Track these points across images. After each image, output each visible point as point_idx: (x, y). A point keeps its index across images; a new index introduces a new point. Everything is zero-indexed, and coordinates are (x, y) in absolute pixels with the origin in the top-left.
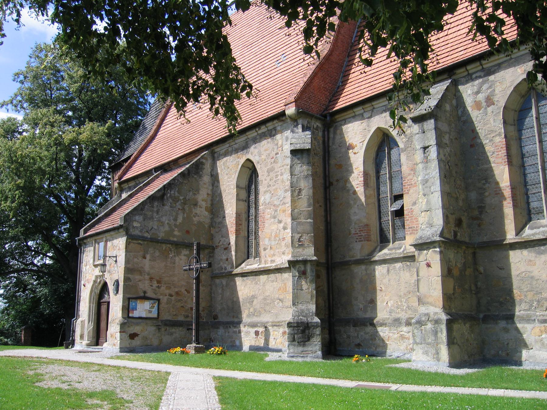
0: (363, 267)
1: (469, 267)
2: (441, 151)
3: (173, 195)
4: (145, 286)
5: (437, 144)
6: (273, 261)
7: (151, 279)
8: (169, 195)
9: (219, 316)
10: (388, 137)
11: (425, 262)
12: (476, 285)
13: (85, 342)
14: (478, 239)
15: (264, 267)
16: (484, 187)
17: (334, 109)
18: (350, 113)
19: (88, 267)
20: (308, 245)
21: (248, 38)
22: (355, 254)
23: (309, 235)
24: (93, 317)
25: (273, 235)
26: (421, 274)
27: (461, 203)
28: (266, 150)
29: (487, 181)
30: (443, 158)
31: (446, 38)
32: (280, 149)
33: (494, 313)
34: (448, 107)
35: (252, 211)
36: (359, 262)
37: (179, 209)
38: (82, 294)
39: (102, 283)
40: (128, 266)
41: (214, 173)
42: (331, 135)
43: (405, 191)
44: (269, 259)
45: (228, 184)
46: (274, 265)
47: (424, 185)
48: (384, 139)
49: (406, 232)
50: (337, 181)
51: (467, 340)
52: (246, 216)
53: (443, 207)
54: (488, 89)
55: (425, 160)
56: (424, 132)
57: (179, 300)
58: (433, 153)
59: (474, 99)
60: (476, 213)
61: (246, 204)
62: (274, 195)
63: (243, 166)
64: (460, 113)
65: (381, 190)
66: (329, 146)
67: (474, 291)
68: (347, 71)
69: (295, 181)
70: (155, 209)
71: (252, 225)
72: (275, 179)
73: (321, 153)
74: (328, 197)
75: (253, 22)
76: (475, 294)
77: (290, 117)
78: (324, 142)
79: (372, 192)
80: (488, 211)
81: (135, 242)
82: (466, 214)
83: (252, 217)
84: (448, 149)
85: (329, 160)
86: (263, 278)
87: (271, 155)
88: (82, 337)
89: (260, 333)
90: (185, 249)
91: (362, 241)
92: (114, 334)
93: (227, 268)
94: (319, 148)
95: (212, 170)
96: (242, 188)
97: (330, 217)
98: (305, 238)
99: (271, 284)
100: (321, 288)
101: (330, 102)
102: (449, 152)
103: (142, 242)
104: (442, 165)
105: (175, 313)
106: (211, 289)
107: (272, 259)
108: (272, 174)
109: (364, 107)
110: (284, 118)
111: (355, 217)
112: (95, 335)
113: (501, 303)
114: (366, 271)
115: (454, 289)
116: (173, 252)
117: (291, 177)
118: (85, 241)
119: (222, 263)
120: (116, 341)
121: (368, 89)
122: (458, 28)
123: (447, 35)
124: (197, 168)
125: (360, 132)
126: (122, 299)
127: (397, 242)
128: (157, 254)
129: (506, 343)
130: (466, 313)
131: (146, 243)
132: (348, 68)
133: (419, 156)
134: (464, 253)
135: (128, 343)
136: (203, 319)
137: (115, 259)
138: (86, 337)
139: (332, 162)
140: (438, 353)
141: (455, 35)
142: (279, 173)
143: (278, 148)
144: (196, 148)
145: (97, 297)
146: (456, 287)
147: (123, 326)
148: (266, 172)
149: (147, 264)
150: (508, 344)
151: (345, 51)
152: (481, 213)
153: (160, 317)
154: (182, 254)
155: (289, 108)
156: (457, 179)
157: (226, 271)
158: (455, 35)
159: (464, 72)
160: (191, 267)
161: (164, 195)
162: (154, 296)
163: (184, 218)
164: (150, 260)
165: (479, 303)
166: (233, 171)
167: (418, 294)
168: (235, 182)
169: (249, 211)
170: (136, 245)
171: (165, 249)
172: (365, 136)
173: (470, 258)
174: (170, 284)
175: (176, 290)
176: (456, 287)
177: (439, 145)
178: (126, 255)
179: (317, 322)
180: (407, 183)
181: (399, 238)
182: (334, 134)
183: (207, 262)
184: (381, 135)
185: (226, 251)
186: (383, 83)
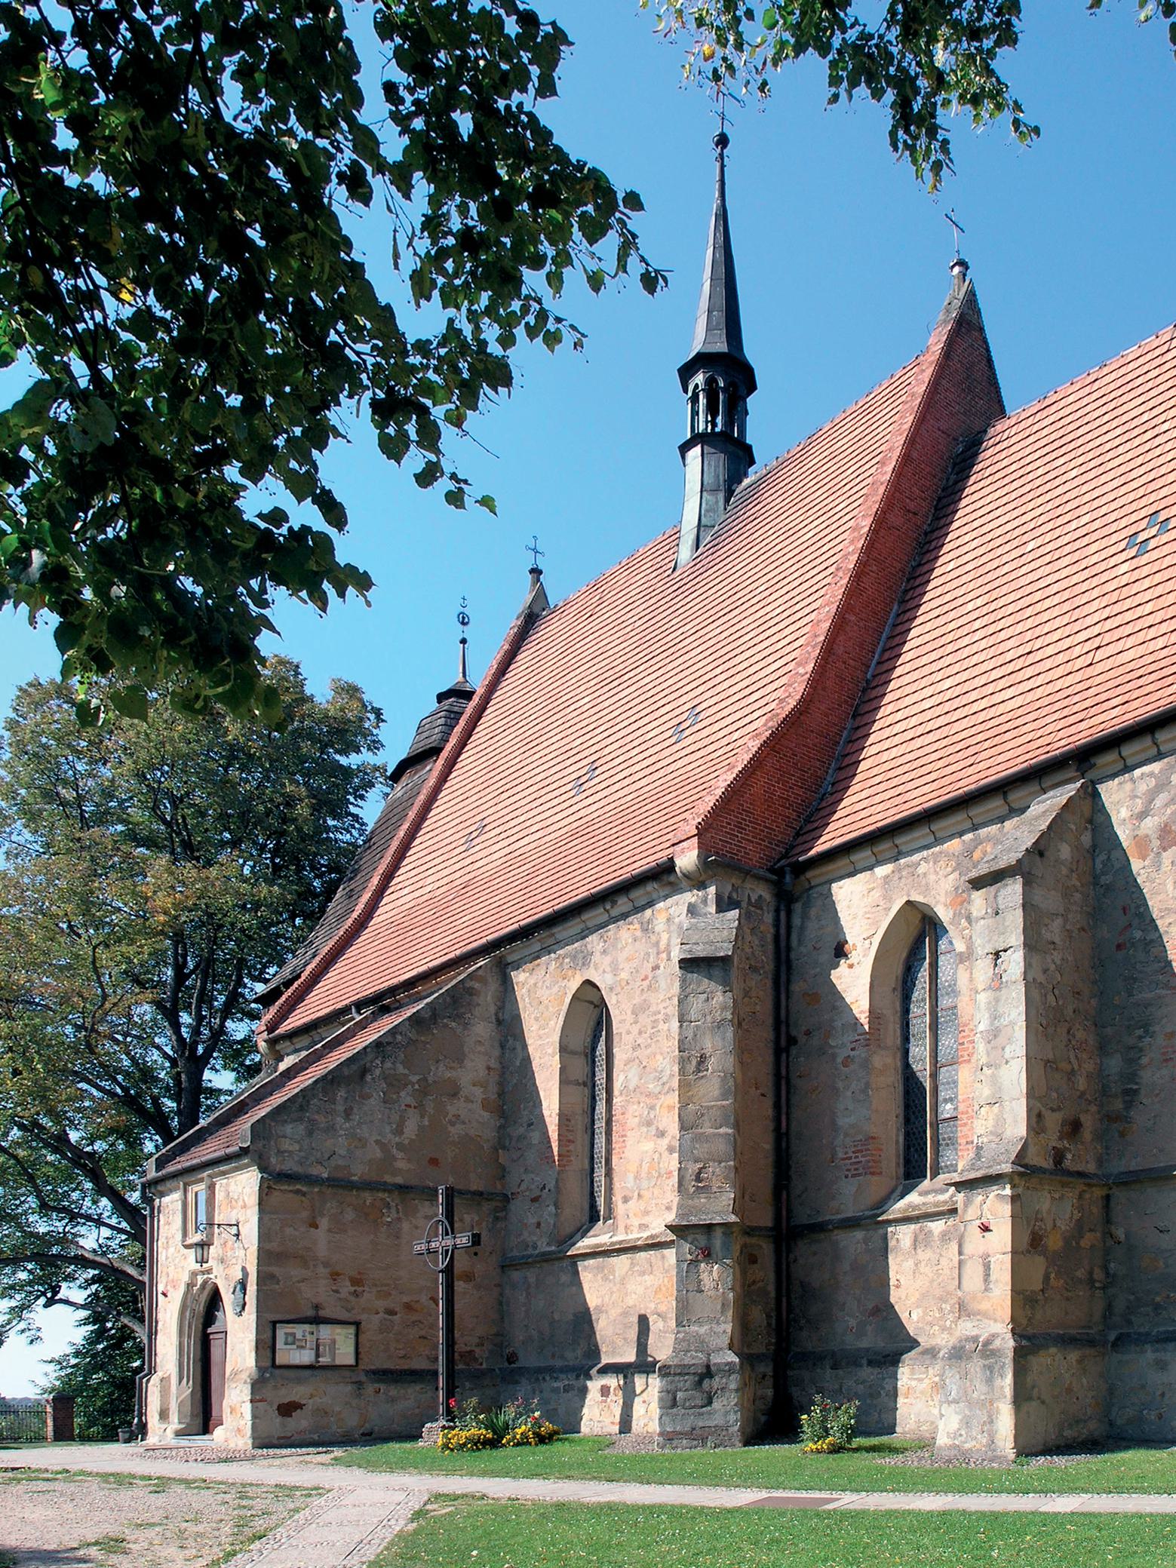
0: (859, 1235)
1: (1091, 1230)
2: (1036, 960)
3: (392, 1072)
4: (318, 1291)
5: (1026, 945)
6: (643, 1227)
7: (335, 1276)
8: (378, 1072)
9: (521, 1355)
10: (936, 924)
11: (978, 1222)
12: (1105, 1268)
13: (175, 1423)
14: (1119, 1166)
15: (621, 1242)
16: (1141, 1045)
17: (812, 852)
18: (842, 863)
19: (172, 1250)
20: (719, 1187)
21: (613, 658)
22: (842, 1206)
23: (723, 1164)
24: (192, 1367)
25: (645, 1166)
26: (968, 1249)
27: (1082, 1083)
28: (628, 960)
29: (1146, 1032)
30: (1041, 978)
31: (1090, 671)
32: (664, 955)
33: (1142, 1330)
34: (1065, 852)
35: (601, 1107)
36: (851, 1224)
37: (409, 1106)
38: (160, 1316)
39: (208, 1288)
40: (268, 1246)
41: (507, 1016)
42: (796, 921)
43: (962, 1056)
44: (635, 1222)
45: (540, 1042)
46: (645, 1235)
47: (989, 1042)
48: (924, 931)
49: (960, 1154)
50: (808, 1033)
51: (1069, 1390)
52: (588, 1120)
53: (1031, 1094)
54: (1166, 805)
55: (997, 983)
56: (997, 913)
57: (413, 1322)
58: (1015, 963)
59: (1134, 830)
60: (1118, 1105)
61: (587, 1091)
62: (648, 1069)
63: (575, 997)
64: (1099, 866)
65: (911, 1055)
66: (789, 948)
67: (1100, 1282)
68: (848, 754)
69: (690, 1036)
70: (340, 1108)
71: (600, 1141)
72: (650, 1031)
73: (770, 967)
74: (784, 1072)
75: (630, 615)
76: (1103, 1288)
77: (687, 876)
78: (777, 938)
79: (889, 1060)
80: (1144, 1101)
81: (286, 1187)
82: (1093, 1108)
83: (600, 1125)
84: (1057, 956)
85: (788, 982)
86: (621, 1262)
87: (644, 972)
88: (164, 1415)
89: (612, 1390)
90: (427, 1203)
91: (859, 1175)
92: (238, 1405)
93: (539, 1243)
94: (764, 952)
95: (501, 1008)
96: (574, 1053)
97: (788, 1119)
98: (714, 1172)
99: (639, 1279)
100: (760, 1284)
101: (798, 834)
102: (1059, 962)
103: (304, 1189)
104: (1036, 994)
105: (402, 1353)
106: (501, 1295)
107: (643, 1222)
108: (645, 1020)
109: (875, 850)
110: (672, 878)
111: (847, 1120)
112: (199, 1409)
113: (1157, 1307)
114: (867, 1245)
115: (1047, 1278)
116: (393, 1210)
117: (681, 1026)
118: (160, 1188)
119: (526, 1234)
120: (243, 1422)
121: (888, 805)
122: (1120, 646)
123: (1091, 664)
124: (458, 1001)
125: (866, 913)
126: (255, 1325)
127: (941, 1176)
128: (350, 1215)
129: (1159, 1393)
130: (1073, 1332)
131: (316, 1190)
132: (850, 748)
133: (983, 969)
134: (1080, 1197)
135: (276, 1425)
136: (481, 1364)
137: (234, 1230)
138: (174, 1417)
139: (797, 987)
140: (991, 1422)
141: (1109, 664)
142: (660, 1017)
143: (658, 954)
144: (458, 952)
145: (196, 1325)
146: (1053, 1275)
147: (257, 1386)
148: (629, 1012)
149: (321, 1240)
150: (1163, 1395)
151: (846, 702)
152: (1129, 1105)
153: (360, 1362)
154: (418, 1215)
155: (683, 851)
156: (1077, 1025)
157: (537, 1252)
158: (1109, 664)
159: (1114, 762)
160: (433, 1245)
161: (364, 1072)
162: (344, 1315)
163: (421, 1128)
164: (329, 1230)
165: (1109, 1307)
166: (551, 1009)
167: (960, 1293)
168: (556, 1038)
169: (593, 1109)
170: (291, 1195)
171: (372, 1205)
172: (876, 923)
173: (1095, 1210)
174: (387, 1285)
175: (406, 1299)
176: (1053, 1275)
177: (1032, 944)
178: (260, 1220)
179: (728, 1364)
180: (969, 1036)
181: (946, 1166)
182: (802, 918)
183: (470, 1234)
184: (916, 920)
185: (537, 1205)
186: (927, 789)
